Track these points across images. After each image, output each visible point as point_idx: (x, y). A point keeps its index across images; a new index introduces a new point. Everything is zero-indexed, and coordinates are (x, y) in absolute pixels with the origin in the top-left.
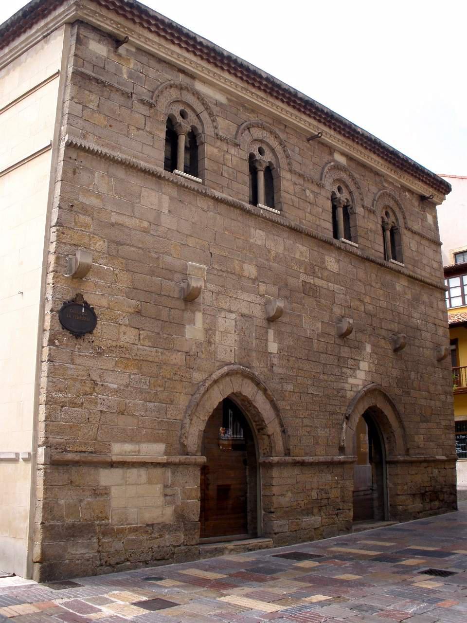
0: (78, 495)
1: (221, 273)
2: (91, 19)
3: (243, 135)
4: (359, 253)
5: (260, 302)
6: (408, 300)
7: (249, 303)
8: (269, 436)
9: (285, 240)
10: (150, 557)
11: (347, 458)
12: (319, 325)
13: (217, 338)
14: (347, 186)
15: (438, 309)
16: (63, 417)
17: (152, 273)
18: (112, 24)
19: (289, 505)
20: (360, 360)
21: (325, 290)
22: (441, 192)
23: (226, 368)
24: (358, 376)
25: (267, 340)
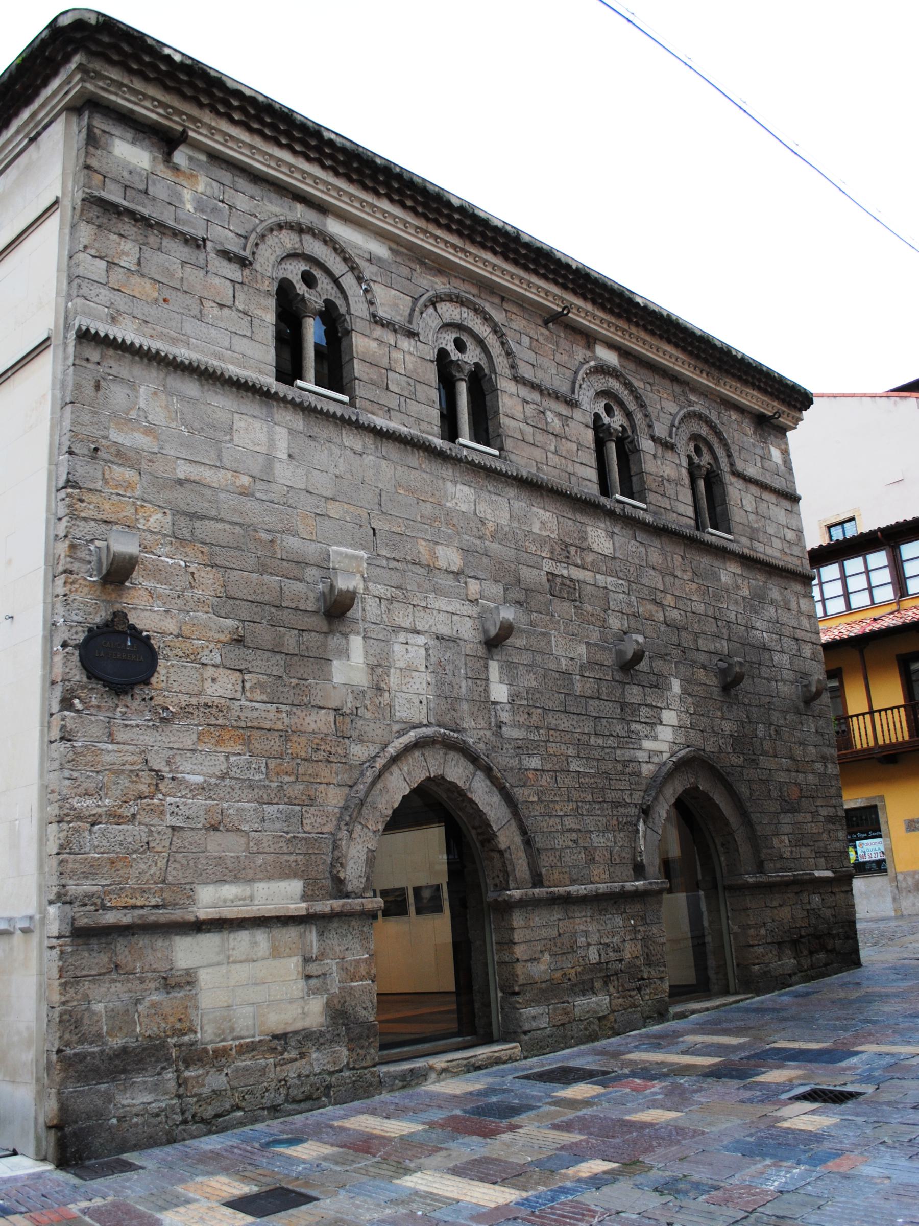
0: (130, 991)
1: (393, 564)
2: (113, 97)
3: (424, 315)
4: (649, 518)
5: (470, 613)
6: (744, 598)
7: (454, 615)
8: (501, 852)
9: (511, 502)
10: (283, 1097)
11: (651, 883)
12: (582, 649)
13: (394, 680)
14: (621, 404)
15: (799, 611)
16: (96, 843)
17: (263, 569)
18: (155, 106)
19: (548, 978)
20: (661, 708)
21: (589, 587)
22: (795, 407)
23: (412, 733)
24: (661, 736)
25: (487, 680)
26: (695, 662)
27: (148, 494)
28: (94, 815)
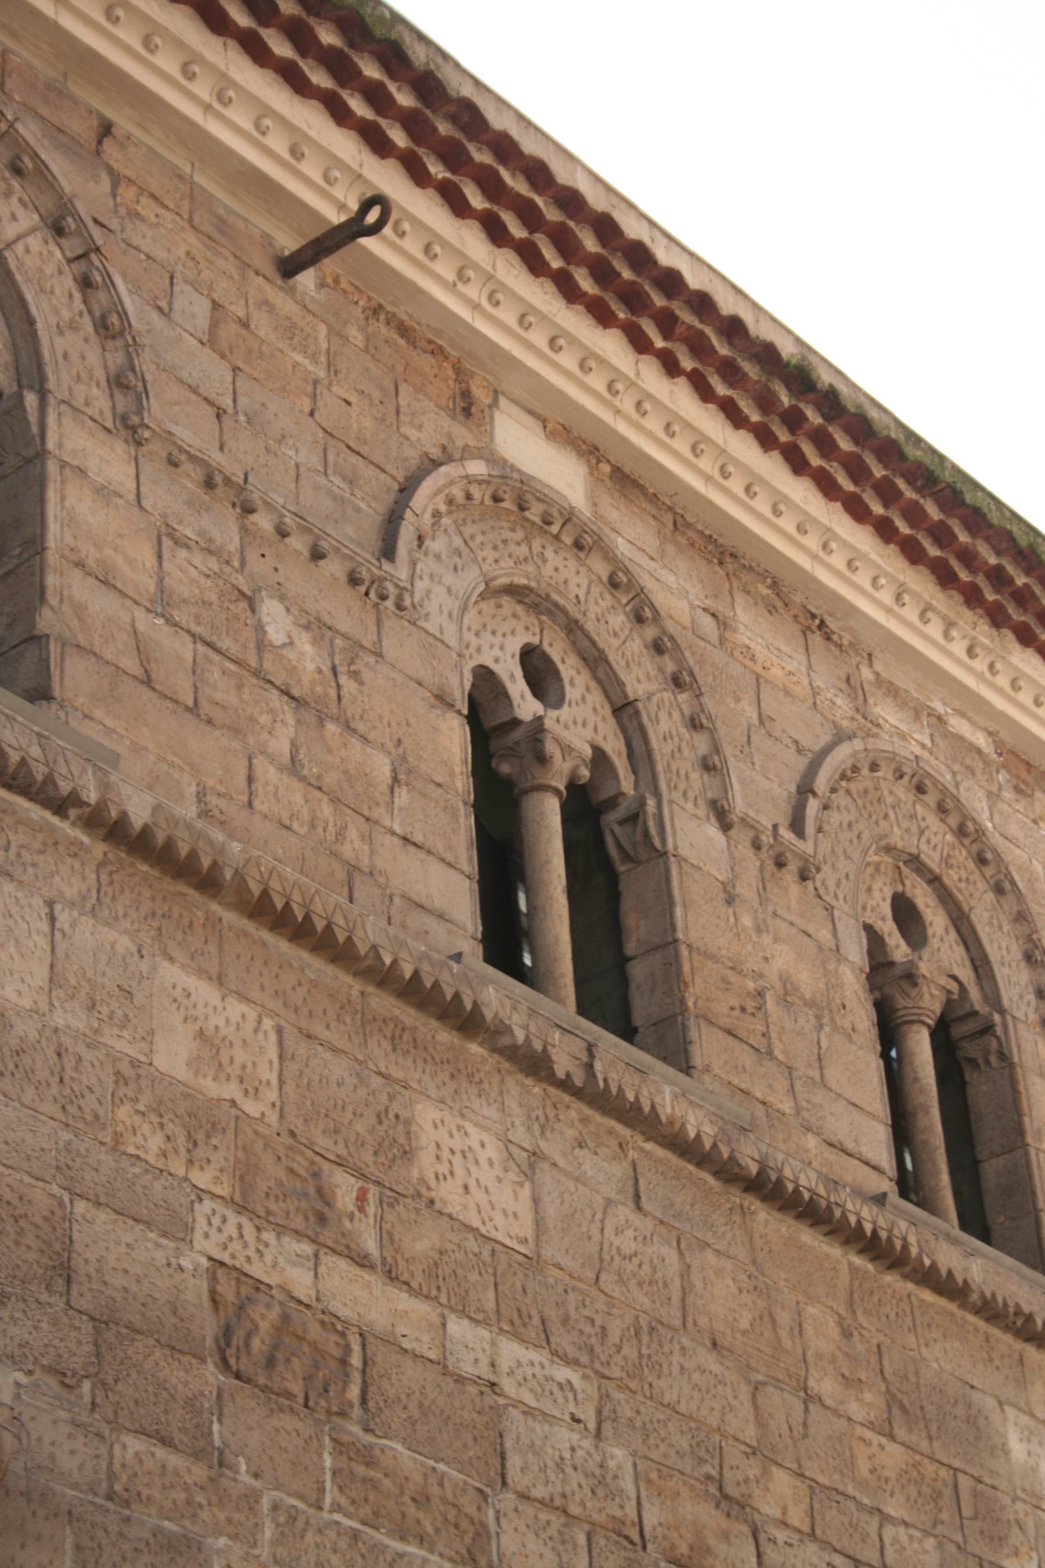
9: (64, 918)
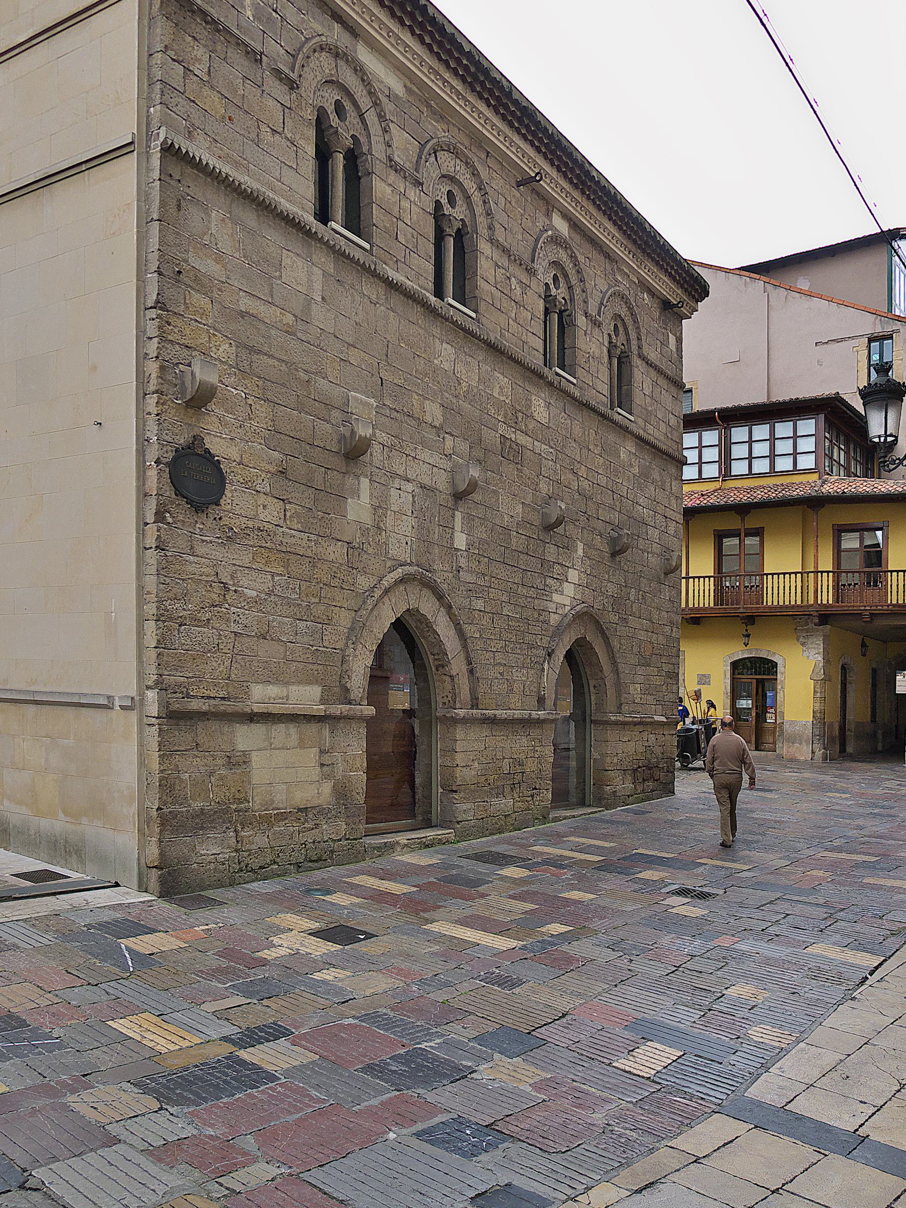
4: (577, 394)
6: (635, 475)
7: (430, 467)
13: (389, 521)
26: (595, 529)
27: (218, 323)
28: (181, 617)
